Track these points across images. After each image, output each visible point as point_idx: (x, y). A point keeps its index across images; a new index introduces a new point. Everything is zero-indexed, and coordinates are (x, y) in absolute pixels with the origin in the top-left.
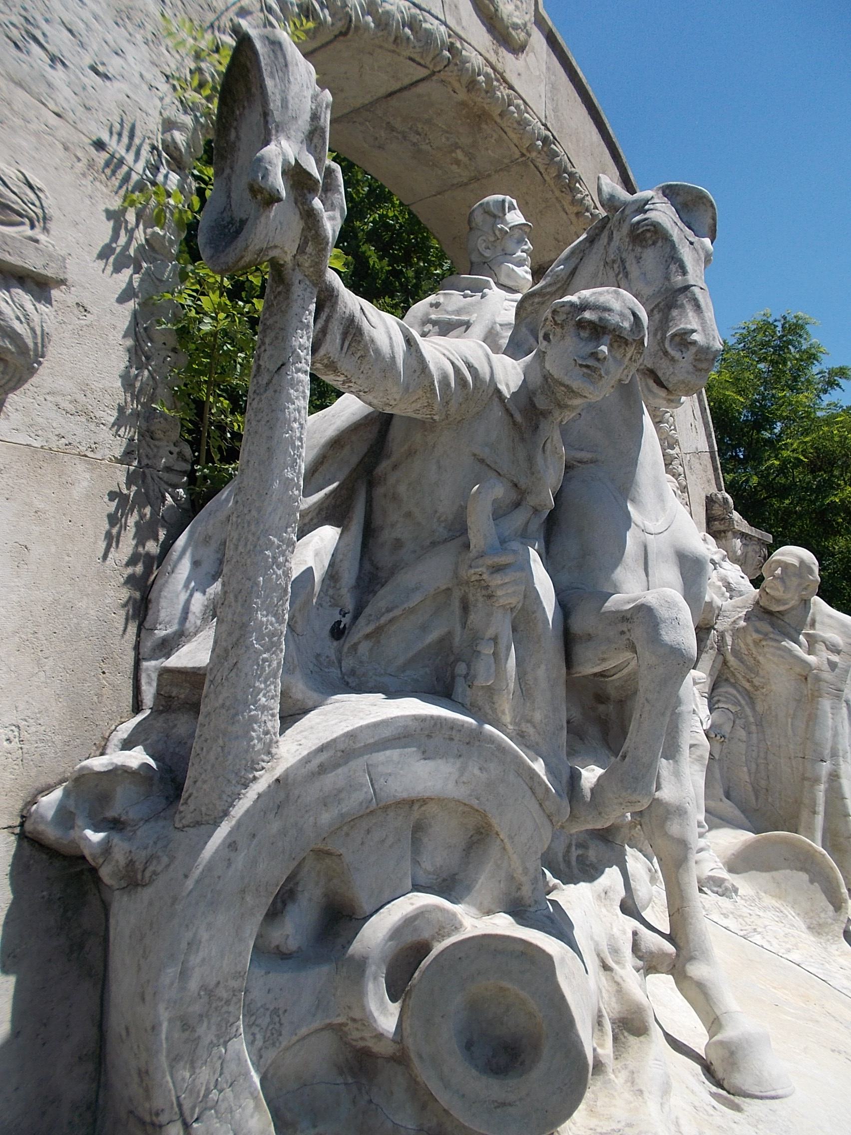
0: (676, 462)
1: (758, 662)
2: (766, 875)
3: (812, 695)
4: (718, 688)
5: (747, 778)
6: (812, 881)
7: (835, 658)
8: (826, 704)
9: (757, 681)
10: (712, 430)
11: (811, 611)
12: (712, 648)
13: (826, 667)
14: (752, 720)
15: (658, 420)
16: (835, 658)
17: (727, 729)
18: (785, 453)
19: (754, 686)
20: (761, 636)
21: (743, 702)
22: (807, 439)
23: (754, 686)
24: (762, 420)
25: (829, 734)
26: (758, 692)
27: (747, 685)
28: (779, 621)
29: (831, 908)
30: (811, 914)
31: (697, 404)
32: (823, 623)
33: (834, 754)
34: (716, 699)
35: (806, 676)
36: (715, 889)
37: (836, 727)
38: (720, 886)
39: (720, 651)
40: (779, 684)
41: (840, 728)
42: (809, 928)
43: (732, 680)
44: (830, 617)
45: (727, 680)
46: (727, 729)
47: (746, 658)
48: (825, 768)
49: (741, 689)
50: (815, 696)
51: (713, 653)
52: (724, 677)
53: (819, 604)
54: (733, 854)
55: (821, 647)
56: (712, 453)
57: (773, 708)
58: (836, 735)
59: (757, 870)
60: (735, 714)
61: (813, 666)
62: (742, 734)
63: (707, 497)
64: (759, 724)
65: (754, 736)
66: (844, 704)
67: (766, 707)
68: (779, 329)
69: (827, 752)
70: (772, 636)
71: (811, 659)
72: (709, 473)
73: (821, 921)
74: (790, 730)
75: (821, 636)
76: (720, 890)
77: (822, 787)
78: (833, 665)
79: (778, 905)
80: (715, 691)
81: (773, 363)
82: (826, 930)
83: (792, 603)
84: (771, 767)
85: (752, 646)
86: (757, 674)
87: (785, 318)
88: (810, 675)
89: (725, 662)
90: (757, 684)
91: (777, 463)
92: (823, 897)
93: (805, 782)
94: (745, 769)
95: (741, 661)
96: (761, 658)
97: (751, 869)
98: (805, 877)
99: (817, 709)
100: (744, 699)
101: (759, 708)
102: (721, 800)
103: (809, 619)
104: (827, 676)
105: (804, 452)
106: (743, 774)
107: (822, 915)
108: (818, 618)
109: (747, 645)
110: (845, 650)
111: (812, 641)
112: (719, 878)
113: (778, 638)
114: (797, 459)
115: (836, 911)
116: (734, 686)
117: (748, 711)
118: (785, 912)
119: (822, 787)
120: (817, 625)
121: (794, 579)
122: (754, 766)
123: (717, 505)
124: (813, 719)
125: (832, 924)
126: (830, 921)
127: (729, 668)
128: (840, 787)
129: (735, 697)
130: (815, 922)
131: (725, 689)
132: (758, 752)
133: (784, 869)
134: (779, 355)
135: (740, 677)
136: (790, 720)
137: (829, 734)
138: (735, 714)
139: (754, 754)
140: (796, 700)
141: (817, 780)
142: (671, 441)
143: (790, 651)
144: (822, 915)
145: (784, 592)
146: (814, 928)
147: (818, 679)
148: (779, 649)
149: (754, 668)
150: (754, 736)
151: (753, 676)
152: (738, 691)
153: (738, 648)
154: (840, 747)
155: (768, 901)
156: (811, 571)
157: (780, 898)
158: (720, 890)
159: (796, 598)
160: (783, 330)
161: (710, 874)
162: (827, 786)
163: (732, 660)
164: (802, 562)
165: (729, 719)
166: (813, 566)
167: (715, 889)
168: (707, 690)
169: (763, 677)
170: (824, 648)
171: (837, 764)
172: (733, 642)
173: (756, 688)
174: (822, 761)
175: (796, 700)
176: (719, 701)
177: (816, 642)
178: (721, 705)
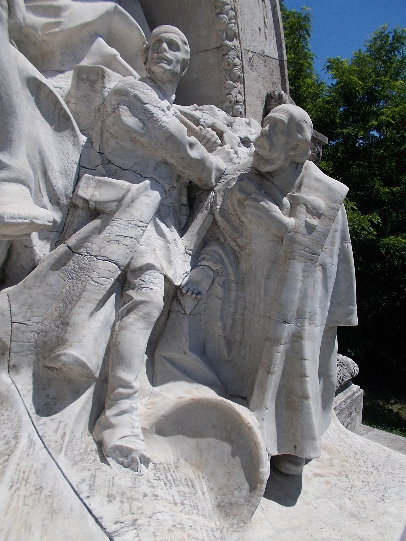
0: (232, 54)
1: (243, 222)
2: (192, 441)
3: (285, 256)
4: (206, 247)
5: (220, 332)
6: (233, 454)
7: (314, 221)
8: (298, 267)
9: (240, 241)
10: (283, 41)
11: (301, 175)
12: (206, 209)
13: (303, 229)
14: (233, 278)
15: (218, 11)
16: (314, 221)
17: (205, 285)
18: (382, 118)
19: (239, 246)
20: (245, 196)
21: (226, 261)
22: (396, 109)
23: (239, 246)
24: (372, 97)
25: (296, 297)
26: (243, 252)
27: (234, 245)
28: (269, 184)
29: (247, 486)
30: (225, 490)
31: (270, 15)
32: (309, 186)
33: (300, 316)
34: (202, 256)
35: (283, 237)
36: (121, 459)
37: (305, 290)
38: (127, 457)
39: (212, 212)
40: (259, 245)
41: (310, 291)
42: (219, 506)
43: (222, 240)
44: (318, 180)
45: (218, 240)
46: (205, 285)
47: (233, 218)
48: (288, 330)
49: (228, 248)
50: (289, 257)
51: (206, 212)
52: (216, 237)
53: (312, 170)
54: (163, 416)
55: (302, 209)
56: (281, 61)
57: (253, 268)
58: (304, 297)
59: (184, 434)
60: (216, 273)
61: (290, 227)
62: (219, 291)
63: (268, 94)
64: (241, 282)
65: (233, 293)
66: (320, 268)
67: (249, 267)
68: (391, 38)
69: (292, 313)
70: (253, 196)
71: (290, 221)
72: (275, 77)
73: (233, 500)
74: (262, 290)
75: (304, 199)
76: (126, 461)
77: (282, 348)
78: (310, 228)
79: (192, 476)
80: (204, 250)
81: (384, 62)
82: (235, 511)
83: (278, 164)
84: (246, 323)
85: (236, 206)
86: (241, 235)
87: (395, 31)
88: (285, 236)
89: (215, 222)
90: (241, 244)
91: (376, 123)
92: (242, 473)
93: (266, 342)
94: (220, 324)
95: (229, 221)
96: (244, 219)
97: (179, 433)
98: (227, 448)
99: (288, 271)
100: (228, 258)
101: (243, 267)
102: (185, 353)
103: (297, 182)
104: (303, 238)
105: (393, 118)
106: (217, 329)
107: (236, 493)
108: (305, 181)
109: (233, 205)
110: (326, 213)
111: (295, 202)
112: (127, 448)
113: (258, 197)
114: (388, 121)
115: (251, 492)
116: (222, 245)
117: (230, 270)
118: (198, 487)
119: (282, 348)
120: (303, 189)
121: (281, 137)
122: (229, 322)
123: (273, 101)
124: (284, 281)
125: (242, 505)
126: (242, 501)
127: (219, 228)
128: (301, 348)
129: (220, 256)
130: (226, 500)
131: (214, 248)
132: (236, 308)
133: (211, 437)
134: (389, 56)
135: (228, 238)
136: (263, 280)
137: (296, 297)
138: (216, 273)
139: (232, 310)
140: (272, 261)
141: (277, 341)
142: (230, 33)
143: (267, 212)
144: (236, 493)
145: (270, 150)
146: (223, 507)
147: (293, 241)
148: (257, 208)
149: (238, 229)
150: (233, 293)
151: (237, 236)
152: (225, 250)
153: (226, 208)
154: (308, 310)
155: (187, 471)
156: (301, 130)
157: (199, 468)
158: (126, 461)
159: (283, 158)
160: (393, 40)
161: (118, 443)
162: (288, 346)
163: (219, 218)
164: (292, 118)
165: (208, 276)
166: (304, 125)
167: (121, 459)
168: (192, 248)
169: (246, 238)
170: (304, 210)
171: (301, 326)
172: (223, 202)
173: (242, 248)
174: (285, 322)
175: (272, 261)
176: (204, 258)
177: (298, 204)
178: (203, 263)
